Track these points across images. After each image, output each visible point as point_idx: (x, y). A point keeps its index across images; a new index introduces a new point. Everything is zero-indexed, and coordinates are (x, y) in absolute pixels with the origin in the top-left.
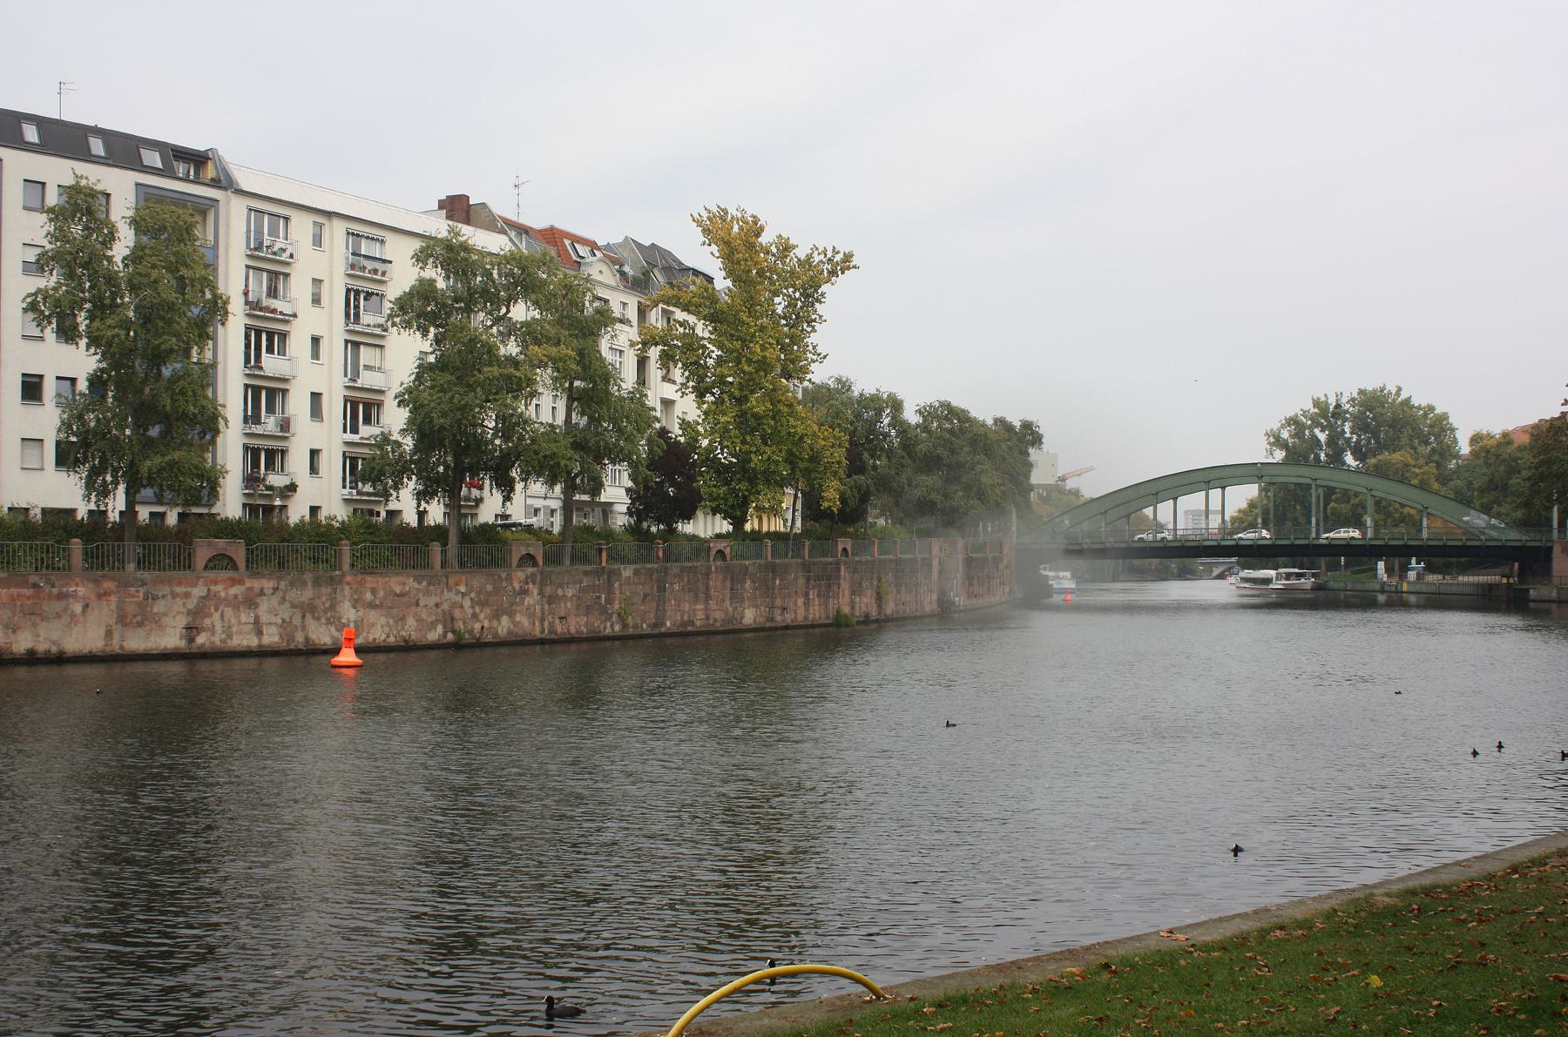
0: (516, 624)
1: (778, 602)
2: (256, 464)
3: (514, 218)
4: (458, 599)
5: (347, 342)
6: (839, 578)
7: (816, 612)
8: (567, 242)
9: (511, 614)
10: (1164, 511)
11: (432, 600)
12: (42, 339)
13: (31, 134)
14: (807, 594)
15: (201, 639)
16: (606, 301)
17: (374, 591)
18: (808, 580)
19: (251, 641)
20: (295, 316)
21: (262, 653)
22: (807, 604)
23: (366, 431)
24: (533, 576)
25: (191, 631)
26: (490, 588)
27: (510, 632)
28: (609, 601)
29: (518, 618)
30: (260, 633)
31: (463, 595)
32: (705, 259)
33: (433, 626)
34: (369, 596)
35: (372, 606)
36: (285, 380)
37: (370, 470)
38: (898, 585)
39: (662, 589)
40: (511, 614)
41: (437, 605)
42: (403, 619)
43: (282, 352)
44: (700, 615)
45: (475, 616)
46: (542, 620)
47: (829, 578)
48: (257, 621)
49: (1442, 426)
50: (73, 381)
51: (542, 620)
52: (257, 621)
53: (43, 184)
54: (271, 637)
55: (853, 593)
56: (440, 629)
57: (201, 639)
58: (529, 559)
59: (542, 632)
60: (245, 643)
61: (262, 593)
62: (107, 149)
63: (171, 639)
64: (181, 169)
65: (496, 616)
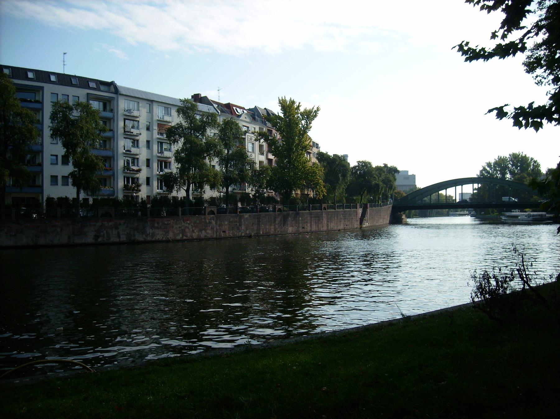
0: (207, 233)
1: (301, 225)
2: (128, 182)
3: (217, 101)
4: (187, 225)
5: (158, 142)
6: (322, 217)
7: (314, 228)
8: (234, 108)
9: (205, 230)
10: (443, 192)
11: (178, 226)
12: (57, 144)
13: (53, 78)
14: (311, 223)
15: (100, 240)
16: (248, 127)
17: (158, 223)
18: (311, 217)
19: (117, 240)
20: (141, 134)
21: (120, 243)
22: (311, 226)
23: (167, 171)
24: (213, 218)
25: (96, 237)
26: (198, 222)
27: (205, 236)
28: (240, 225)
29: (208, 231)
30: (119, 237)
31: (189, 224)
32: (277, 110)
33: (179, 234)
34: (156, 225)
35: (157, 228)
36: (137, 155)
37: (168, 181)
38: (345, 219)
39: (259, 221)
40: (205, 230)
41: (180, 227)
42: (168, 232)
43: (138, 147)
44: (273, 230)
45: (193, 231)
46: (217, 232)
47: (319, 217)
48: (118, 233)
49: (537, 166)
50: (57, 156)
51: (217, 232)
52: (118, 233)
53: (68, 96)
54: (123, 238)
55: (328, 222)
56: (181, 235)
57: (100, 240)
58: (212, 213)
59: (217, 235)
60: (115, 240)
61: (120, 224)
62: (27, 75)
63: (90, 239)
64: (102, 87)
65: (201, 230)
